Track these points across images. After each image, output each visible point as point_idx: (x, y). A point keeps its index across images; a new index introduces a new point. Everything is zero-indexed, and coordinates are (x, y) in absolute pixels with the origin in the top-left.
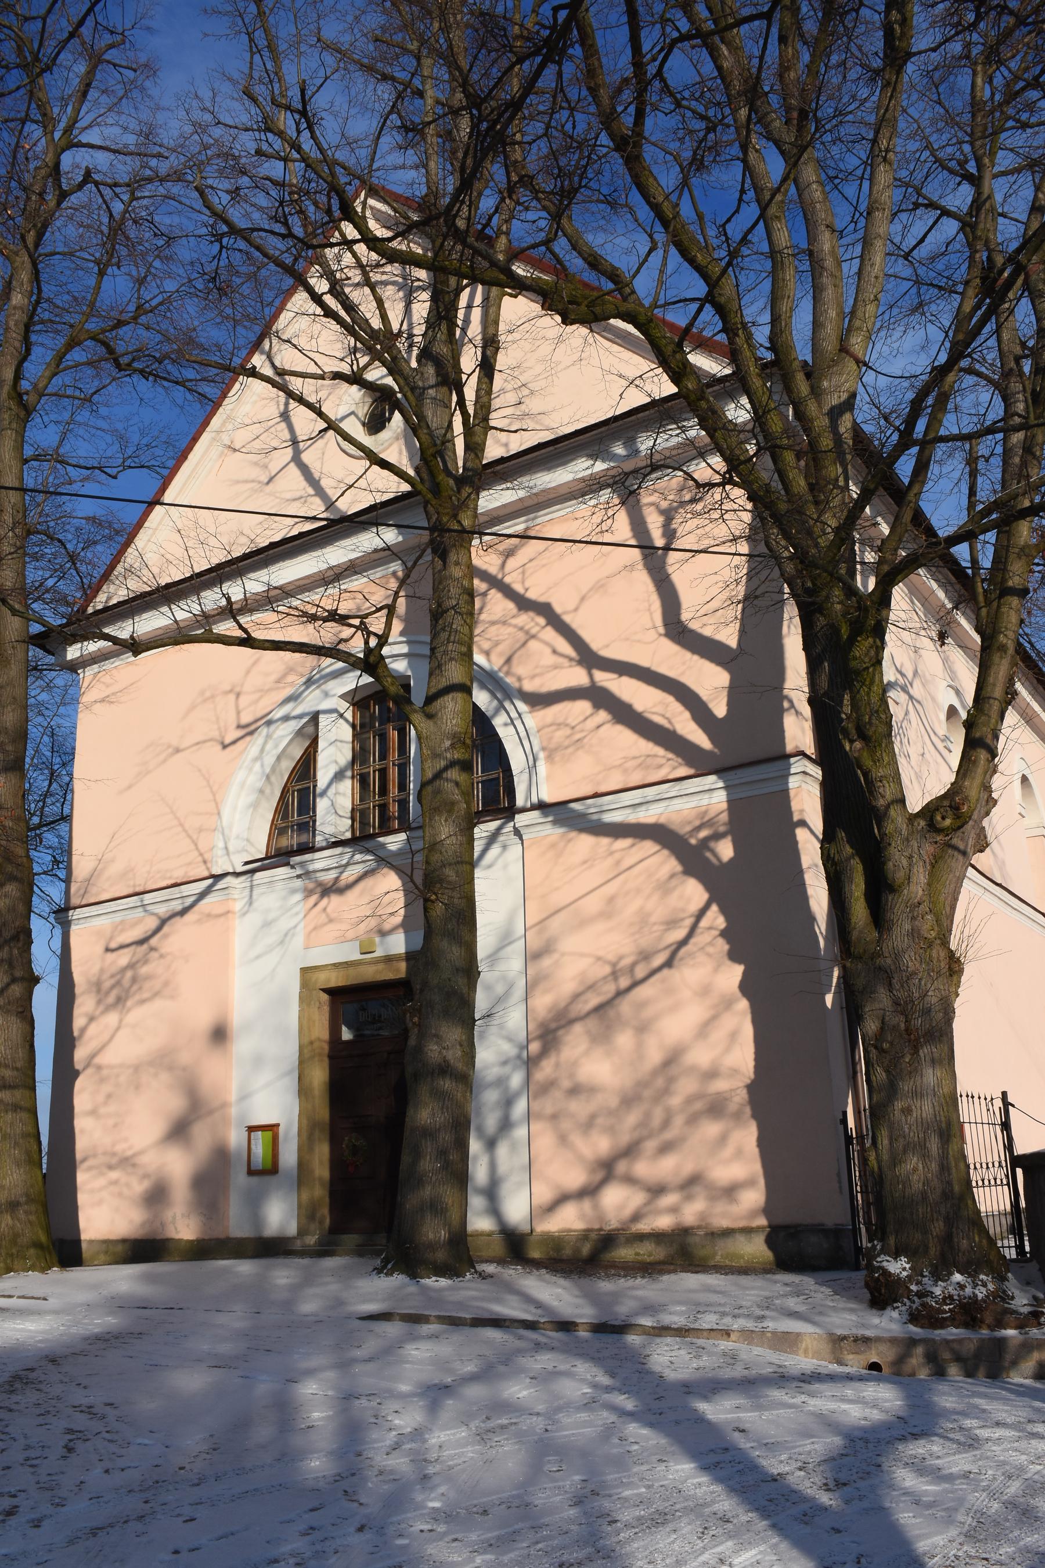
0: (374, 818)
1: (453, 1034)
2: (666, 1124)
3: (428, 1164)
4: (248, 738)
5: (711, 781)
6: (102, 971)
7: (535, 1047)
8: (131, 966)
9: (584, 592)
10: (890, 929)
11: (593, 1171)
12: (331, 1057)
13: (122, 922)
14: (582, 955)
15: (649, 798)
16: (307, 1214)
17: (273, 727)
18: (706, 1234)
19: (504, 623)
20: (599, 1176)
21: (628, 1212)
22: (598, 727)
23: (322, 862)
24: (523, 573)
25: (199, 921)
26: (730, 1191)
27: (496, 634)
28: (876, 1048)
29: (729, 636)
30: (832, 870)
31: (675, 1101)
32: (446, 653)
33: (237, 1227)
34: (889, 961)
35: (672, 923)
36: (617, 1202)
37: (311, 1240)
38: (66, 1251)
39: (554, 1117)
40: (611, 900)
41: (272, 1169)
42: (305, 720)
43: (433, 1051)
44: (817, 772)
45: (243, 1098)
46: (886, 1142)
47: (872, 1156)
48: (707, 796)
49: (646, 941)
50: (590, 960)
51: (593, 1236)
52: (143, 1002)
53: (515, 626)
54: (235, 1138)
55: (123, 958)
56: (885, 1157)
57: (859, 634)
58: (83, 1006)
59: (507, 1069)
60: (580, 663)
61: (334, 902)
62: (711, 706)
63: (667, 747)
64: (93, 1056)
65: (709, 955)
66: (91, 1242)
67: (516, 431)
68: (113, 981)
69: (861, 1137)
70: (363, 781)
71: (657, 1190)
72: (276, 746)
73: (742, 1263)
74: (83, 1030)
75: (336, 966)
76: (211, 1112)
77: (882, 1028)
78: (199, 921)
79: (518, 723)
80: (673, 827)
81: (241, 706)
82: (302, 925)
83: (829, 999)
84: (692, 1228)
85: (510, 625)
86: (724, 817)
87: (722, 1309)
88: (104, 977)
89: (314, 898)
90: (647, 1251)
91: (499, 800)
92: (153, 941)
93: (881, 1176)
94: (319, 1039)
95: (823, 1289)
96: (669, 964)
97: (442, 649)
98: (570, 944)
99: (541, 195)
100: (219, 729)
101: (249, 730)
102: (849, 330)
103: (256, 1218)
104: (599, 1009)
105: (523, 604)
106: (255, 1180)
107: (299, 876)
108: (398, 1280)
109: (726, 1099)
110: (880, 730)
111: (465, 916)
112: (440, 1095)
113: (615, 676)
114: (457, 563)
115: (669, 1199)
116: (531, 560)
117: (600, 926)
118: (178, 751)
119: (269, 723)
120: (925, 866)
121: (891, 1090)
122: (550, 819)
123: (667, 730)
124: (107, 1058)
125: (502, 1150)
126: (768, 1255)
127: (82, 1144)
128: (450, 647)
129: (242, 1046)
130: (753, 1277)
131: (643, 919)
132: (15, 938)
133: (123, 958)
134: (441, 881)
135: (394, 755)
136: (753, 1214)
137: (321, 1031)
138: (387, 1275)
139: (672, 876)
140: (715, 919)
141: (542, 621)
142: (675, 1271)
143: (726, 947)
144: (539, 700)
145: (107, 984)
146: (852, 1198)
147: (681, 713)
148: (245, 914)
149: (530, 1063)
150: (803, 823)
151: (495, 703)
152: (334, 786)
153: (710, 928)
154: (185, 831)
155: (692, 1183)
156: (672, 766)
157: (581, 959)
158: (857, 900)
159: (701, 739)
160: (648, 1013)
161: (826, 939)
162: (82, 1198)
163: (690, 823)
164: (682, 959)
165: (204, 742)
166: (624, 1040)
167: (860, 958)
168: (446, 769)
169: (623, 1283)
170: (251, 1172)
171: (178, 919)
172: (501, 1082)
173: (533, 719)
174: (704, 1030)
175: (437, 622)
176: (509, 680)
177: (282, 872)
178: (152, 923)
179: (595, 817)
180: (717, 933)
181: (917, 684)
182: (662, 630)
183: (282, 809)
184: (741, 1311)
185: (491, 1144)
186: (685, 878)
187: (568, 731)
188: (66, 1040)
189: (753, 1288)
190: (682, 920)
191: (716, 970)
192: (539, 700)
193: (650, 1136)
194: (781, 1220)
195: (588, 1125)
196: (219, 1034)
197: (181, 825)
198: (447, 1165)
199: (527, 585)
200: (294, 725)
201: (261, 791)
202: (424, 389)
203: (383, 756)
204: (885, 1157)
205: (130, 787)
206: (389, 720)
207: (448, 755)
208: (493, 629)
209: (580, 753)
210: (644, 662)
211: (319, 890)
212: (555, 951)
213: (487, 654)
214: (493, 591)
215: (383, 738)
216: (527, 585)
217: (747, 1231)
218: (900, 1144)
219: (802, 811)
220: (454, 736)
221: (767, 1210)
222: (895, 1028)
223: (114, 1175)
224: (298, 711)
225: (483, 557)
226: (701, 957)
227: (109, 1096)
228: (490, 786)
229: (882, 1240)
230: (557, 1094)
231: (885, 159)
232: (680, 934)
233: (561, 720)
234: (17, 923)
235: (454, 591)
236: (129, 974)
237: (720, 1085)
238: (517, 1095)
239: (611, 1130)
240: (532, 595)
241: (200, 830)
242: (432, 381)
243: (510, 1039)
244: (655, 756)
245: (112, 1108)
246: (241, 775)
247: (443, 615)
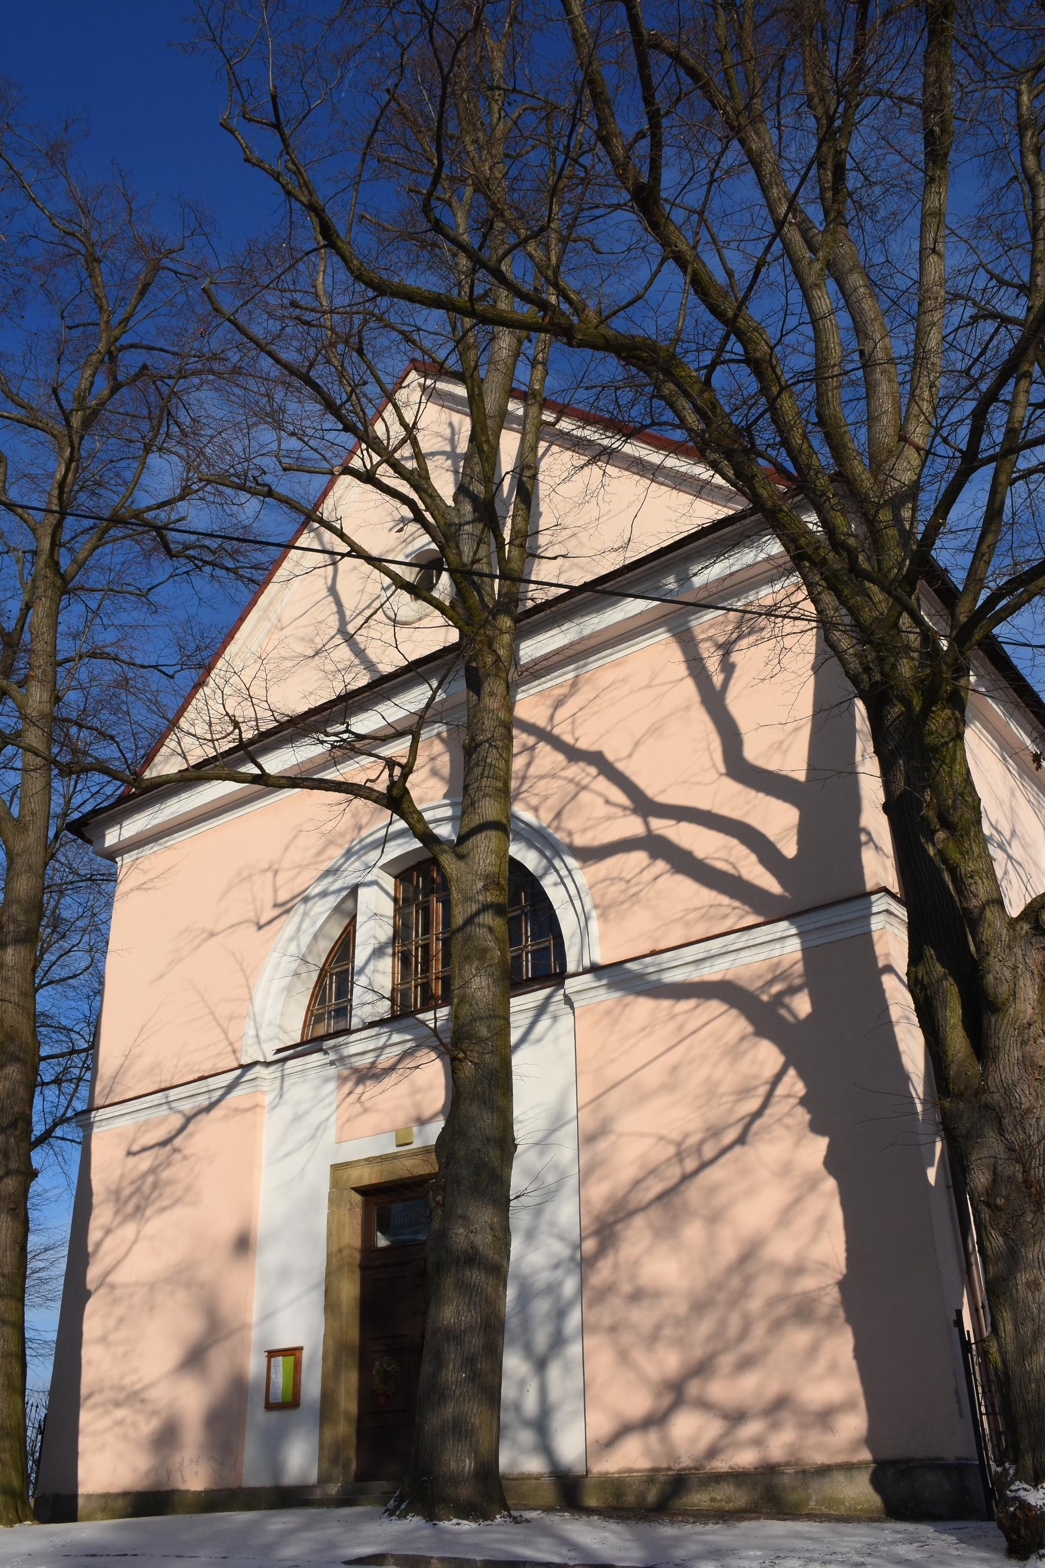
0: (416, 998)
1: (483, 1216)
2: (744, 1333)
3: (453, 1374)
4: (284, 917)
5: (783, 927)
6: (122, 1177)
7: (590, 1245)
8: (153, 1170)
9: (638, 737)
10: (994, 1060)
11: (658, 1395)
12: (363, 1267)
13: (146, 1122)
14: (642, 1135)
15: (713, 952)
16: (330, 1456)
17: (310, 904)
18: (797, 1473)
19: (554, 776)
20: (667, 1400)
21: (702, 1445)
22: (656, 878)
23: (358, 1046)
24: (573, 723)
25: (226, 1117)
26: (825, 1417)
27: (542, 782)
28: (988, 1205)
29: (794, 764)
30: (921, 996)
31: (755, 1305)
32: (479, 789)
33: (252, 1474)
34: (997, 1097)
35: (744, 1092)
36: (690, 1432)
37: (333, 1489)
38: (59, 1505)
39: (613, 1329)
40: (674, 1069)
41: (293, 1402)
42: (344, 893)
43: (460, 1236)
44: (902, 912)
45: (267, 1316)
46: (1009, 1327)
47: (994, 1349)
48: (778, 945)
49: (715, 1114)
50: (653, 1140)
51: (661, 1477)
52: (163, 1210)
53: (565, 778)
54: (254, 1365)
55: (145, 1162)
56: (1010, 1348)
57: (934, 703)
58: (101, 1217)
59: (559, 1273)
60: (635, 811)
61: (370, 1090)
62: (779, 846)
63: (732, 895)
64: (107, 1274)
65: (787, 1127)
66: (89, 1496)
67: (555, 558)
68: (132, 1188)
69: (980, 1340)
70: (405, 960)
71: (736, 1417)
72: (313, 924)
73: (842, 1511)
74: (98, 1245)
75: (369, 1160)
76: (229, 1335)
77: (994, 1181)
78: (226, 1117)
79: (568, 881)
80: (741, 983)
81: (278, 884)
82: (334, 1117)
83: (932, 1174)
84: (779, 1465)
85: (560, 778)
86: (799, 968)
87: (808, 1555)
88: (125, 1183)
89: (349, 1086)
90: (726, 1495)
91: (550, 971)
92: (177, 1142)
93: (1006, 1374)
94: (350, 1247)
95: (945, 1537)
96: (741, 1140)
97: (475, 785)
98: (629, 1122)
100: (255, 909)
101: (285, 908)
102: (907, 418)
103: (276, 1465)
104: (662, 1197)
105: (574, 754)
106: (274, 1415)
107: (332, 1063)
108: (414, 1522)
109: (814, 1300)
110: (967, 816)
111: (500, 1081)
112: (466, 1289)
113: (673, 822)
114: (492, 694)
115: (752, 1428)
116: (581, 709)
117: (662, 1101)
118: (212, 935)
119: (306, 900)
120: (1033, 979)
121: (1013, 1258)
122: (604, 982)
123: (732, 876)
124: (122, 1276)
125: (554, 1372)
126: (875, 1500)
127: (88, 1377)
128: (484, 782)
129: (268, 1257)
130: (855, 1525)
131: (711, 1091)
132: (14, 1125)
133: (145, 1162)
134: (470, 1036)
135: (437, 928)
136: (855, 1446)
137: (352, 1237)
138: (400, 1517)
139: (743, 1038)
140: (793, 1084)
141: (593, 770)
142: (757, 1518)
143: (807, 1117)
144: (590, 855)
145: (127, 1192)
146: (977, 1424)
147: (746, 857)
148: (274, 1107)
149: (584, 1265)
150: (889, 969)
151: (545, 862)
152: (372, 963)
154: (215, 1019)
155: (778, 1407)
156: (734, 913)
157: (642, 1139)
158: (953, 1027)
159: (771, 884)
160: (721, 1198)
161: (924, 1103)
162: (84, 1443)
163: (760, 977)
164: (756, 1134)
165: (239, 924)
166: (693, 1232)
167: (960, 1096)
168: (478, 913)
169: (688, 1528)
170: (270, 1406)
171: (203, 1115)
172: (552, 1289)
173: (583, 875)
174: (785, 1217)
175: (470, 757)
176: (559, 836)
177: (316, 1058)
178: (177, 1121)
179: (654, 977)
180: (796, 1101)
181: (1015, 843)
182: (722, 769)
183: (319, 992)
184: (834, 1557)
185: (541, 1365)
186: (756, 1039)
187: (622, 885)
188: (79, 1256)
189: (853, 1535)
190: (755, 1088)
191: (797, 1144)
192: (590, 855)
193: (725, 1349)
195: (653, 1338)
196: (243, 1244)
197: (212, 1013)
198: (474, 1376)
199: (577, 734)
200: (332, 901)
201: (297, 974)
202: (460, 525)
203: (426, 930)
204: (1010, 1348)
205: (162, 976)
206: (432, 891)
207: (481, 898)
208: (542, 784)
209: (636, 908)
210: (704, 805)
211: (354, 1078)
212: (611, 1132)
213: (536, 810)
214: (541, 744)
215: (426, 911)
216: (577, 734)
217: (848, 1468)
218: (1028, 1330)
219: (887, 955)
220: (487, 876)
221: (871, 1440)
222: (1011, 1179)
223: (120, 1413)
224: (337, 885)
225: (530, 704)
226: (778, 1131)
227: (121, 1320)
228: (540, 955)
229: (1015, 1461)
230: (615, 1302)
231: (934, 251)
232: (753, 1104)
233: (615, 874)
234: (16, 1109)
235: (488, 723)
236: (150, 1179)
237: (808, 1283)
238: (570, 1304)
239: (679, 1342)
240: (582, 745)
241: (231, 1018)
242: (469, 517)
243: (561, 1238)
244: (720, 905)
245: (121, 1334)
246: (273, 958)
247: (482, 760)
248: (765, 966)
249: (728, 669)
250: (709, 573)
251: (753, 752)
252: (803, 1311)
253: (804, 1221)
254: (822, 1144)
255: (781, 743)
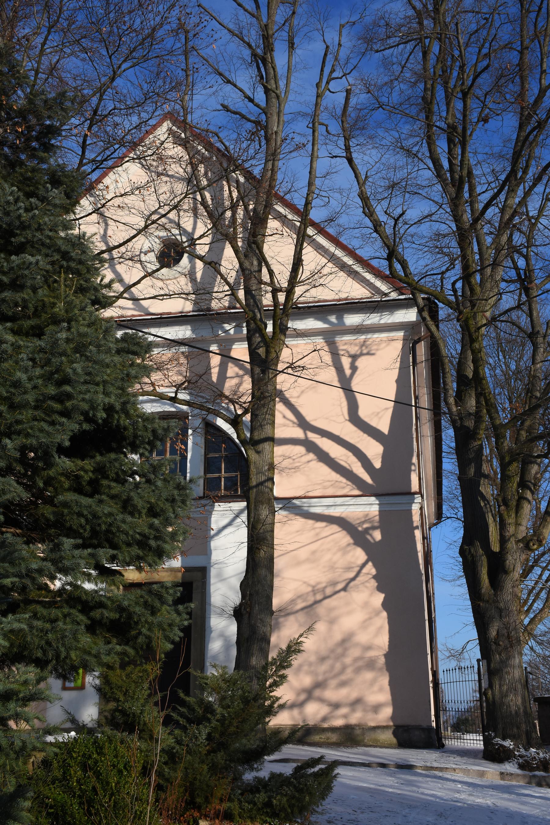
5: (373, 499)
11: (298, 694)
14: (295, 580)
20: (303, 697)
22: (309, 462)
26: (376, 708)
29: (384, 425)
31: (348, 660)
35: (348, 569)
40: (314, 552)
62: (373, 461)
63: (348, 479)
71: (336, 706)
86: (377, 518)
99: (467, 217)
115: (344, 711)
123: (348, 470)
126: (394, 741)
139: (349, 545)
143: (376, 584)
153: (368, 574)
155: (357, 703)
156: (349, 488)
159: (368, 479)
163: (358, 519)
174: (365, 625)
179: (306, 508)
182: (347, 418)
186: (354, 546)
191: (371, 595)
194: (400, 722)
209: (298, 474)
210: (336, 432)
221: (393, 718)
232: (352, 575)
237: (371, 654)
248: (361, 515)
249: (354, 369)
250: (352, 319)
251: (362, 413)
252: (370, 665)
253: (372, 629)
254: (382, 596)
255: (378, 413)
